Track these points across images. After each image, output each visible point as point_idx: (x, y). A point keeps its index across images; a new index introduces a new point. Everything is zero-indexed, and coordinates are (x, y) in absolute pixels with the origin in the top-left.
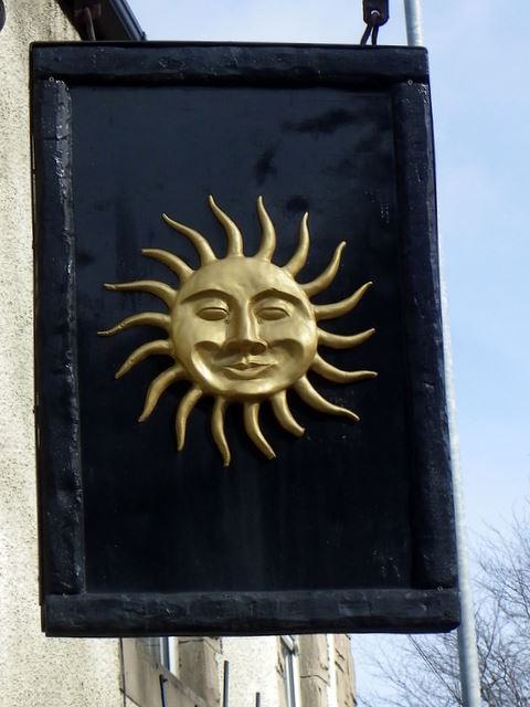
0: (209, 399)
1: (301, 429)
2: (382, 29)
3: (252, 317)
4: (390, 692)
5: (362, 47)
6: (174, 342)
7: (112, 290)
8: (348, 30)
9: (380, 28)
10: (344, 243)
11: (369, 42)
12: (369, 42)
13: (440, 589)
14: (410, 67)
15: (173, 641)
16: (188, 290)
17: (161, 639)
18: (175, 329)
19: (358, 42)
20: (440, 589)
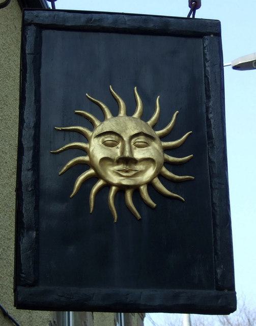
0: (122, 189)
1: (155, 205)
2: (197, 11)
3: (122, 147)
4: (219, 324)
5: (188, 18)
6: (33, 147)
7: (59, 130)
8: (181, 10)
9: (197, 11)
10: (135, 88)
11: (191, 17)
12: (191, 17)
13: (226, 291)
14: (213, 29)
15: (71, 312)
16: (98, 130)
17: (67, 312)
18: (91, 150)
19: (186, 16)
20: (226, 291)
